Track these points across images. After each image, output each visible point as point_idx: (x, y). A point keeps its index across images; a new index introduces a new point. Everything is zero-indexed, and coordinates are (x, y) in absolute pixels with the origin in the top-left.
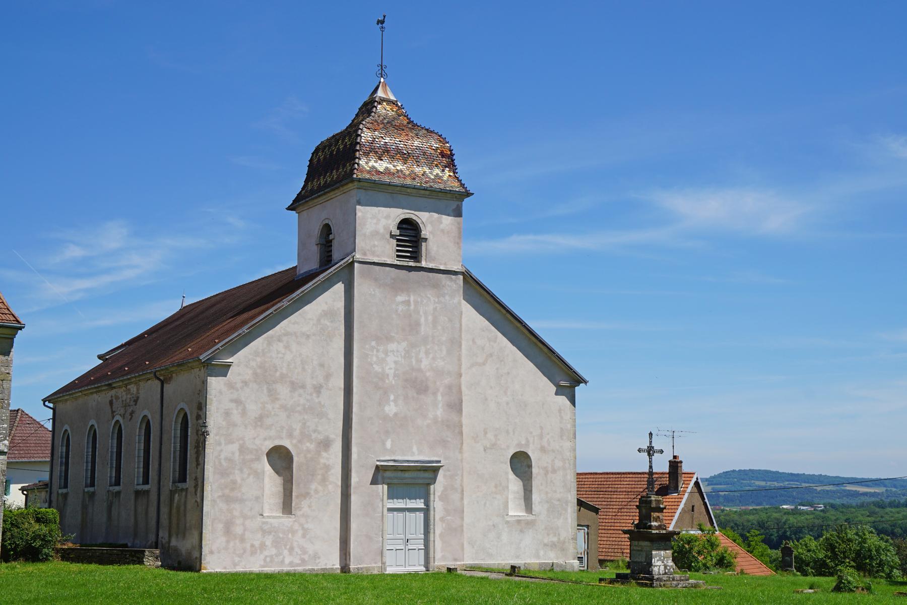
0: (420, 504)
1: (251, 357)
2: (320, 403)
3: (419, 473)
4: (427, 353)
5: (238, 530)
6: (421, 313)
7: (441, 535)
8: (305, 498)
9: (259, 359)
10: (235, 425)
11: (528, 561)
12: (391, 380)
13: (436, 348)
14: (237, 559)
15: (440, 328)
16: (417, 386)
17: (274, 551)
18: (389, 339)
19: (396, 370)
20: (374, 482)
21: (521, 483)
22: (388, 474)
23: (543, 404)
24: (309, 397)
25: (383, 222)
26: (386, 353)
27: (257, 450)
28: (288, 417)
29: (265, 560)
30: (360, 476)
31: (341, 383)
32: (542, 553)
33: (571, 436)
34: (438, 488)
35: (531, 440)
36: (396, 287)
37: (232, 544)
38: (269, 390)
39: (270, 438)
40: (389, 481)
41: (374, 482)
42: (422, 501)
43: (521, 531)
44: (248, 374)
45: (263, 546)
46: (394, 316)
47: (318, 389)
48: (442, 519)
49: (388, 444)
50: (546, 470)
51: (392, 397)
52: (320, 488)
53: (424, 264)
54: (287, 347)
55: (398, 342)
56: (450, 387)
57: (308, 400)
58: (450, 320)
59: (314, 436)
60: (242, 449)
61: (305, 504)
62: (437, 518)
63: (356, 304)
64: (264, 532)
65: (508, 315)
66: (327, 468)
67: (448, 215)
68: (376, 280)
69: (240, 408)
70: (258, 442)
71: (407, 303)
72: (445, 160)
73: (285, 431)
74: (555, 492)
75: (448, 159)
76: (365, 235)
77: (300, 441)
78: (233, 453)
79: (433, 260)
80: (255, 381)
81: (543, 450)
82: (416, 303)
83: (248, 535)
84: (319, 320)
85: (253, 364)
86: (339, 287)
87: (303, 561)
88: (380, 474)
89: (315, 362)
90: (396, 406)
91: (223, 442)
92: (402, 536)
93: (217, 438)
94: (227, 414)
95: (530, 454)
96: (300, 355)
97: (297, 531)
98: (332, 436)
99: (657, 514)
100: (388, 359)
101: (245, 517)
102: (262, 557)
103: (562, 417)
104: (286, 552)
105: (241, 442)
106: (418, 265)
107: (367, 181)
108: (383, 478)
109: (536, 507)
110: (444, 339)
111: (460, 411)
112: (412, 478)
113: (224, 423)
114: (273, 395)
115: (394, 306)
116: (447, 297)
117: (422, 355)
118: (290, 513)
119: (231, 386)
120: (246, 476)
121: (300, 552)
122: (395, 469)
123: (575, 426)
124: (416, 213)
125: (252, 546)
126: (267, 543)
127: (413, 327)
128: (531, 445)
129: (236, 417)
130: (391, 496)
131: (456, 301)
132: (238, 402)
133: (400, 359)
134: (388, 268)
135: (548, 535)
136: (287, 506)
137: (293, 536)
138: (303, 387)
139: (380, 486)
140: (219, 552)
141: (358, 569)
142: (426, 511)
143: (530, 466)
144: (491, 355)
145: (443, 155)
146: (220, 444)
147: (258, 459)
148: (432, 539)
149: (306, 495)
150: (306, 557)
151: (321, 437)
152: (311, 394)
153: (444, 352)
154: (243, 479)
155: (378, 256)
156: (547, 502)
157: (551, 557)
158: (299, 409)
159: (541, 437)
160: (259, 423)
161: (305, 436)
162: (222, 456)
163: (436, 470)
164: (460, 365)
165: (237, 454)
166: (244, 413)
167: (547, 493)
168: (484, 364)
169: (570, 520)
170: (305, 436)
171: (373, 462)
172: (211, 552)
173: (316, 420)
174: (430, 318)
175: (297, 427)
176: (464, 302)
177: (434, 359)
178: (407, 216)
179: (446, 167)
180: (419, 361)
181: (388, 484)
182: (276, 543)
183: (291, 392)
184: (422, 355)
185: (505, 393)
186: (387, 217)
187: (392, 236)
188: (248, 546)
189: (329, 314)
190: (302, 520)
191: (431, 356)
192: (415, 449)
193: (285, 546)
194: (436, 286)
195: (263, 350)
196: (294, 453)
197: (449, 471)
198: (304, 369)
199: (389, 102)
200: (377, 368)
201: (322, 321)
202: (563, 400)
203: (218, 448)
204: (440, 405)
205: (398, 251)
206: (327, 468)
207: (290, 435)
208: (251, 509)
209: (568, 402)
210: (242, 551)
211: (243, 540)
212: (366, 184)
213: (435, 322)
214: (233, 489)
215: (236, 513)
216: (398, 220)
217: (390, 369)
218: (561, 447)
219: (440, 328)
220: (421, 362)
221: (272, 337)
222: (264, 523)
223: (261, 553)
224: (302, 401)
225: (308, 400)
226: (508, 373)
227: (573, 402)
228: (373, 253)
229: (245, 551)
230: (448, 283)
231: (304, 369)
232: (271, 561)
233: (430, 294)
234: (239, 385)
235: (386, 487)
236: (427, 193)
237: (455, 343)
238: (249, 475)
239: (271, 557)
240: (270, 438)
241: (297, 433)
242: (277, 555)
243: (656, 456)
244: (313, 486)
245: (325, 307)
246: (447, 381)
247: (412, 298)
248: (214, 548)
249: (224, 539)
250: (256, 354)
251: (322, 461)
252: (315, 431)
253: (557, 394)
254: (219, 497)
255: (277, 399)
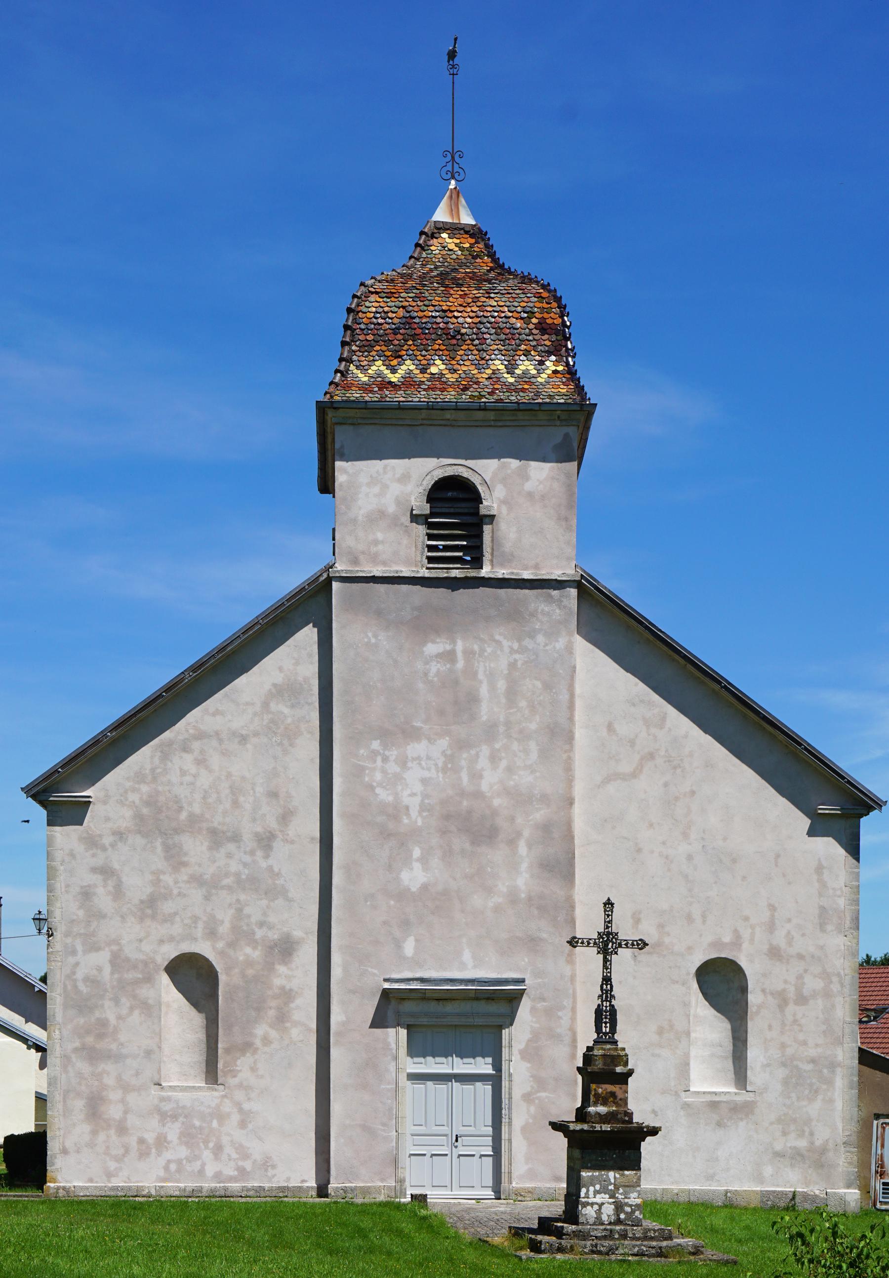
0: (483, 1066)
1: (128, 784)
2: (270, 869)
3: (475, 1004)
4: (494, 758)
5: (114, 1112)
6: (481, 676)
7: (524, 1129)
8: (244, 1055)
9: (145, 788)
10: (102, 916)
11: (735, 1187)
12: (415, 818)
13: (515, 746)
14: (112, 1165)
15: (523, 704)
16: (471, 827)
17: (183, 1152)
18: (411, 734)
19: (425, 796)
20: (379, 1021)
21: (728, 1026)
22: (409, 1007)
23: (778, 856)
24: (247, 859)
25: (396, 489)
26: (403, 763)
27: (146, 964)
28: (207, 898)
29: (166, 1168)
30: (351, 1011)
31: (314, 828)
32: (768, 1171)
33: (848, 924)
34: (518, 1035)
35: (746, 934)
36: (422, 626)
37: (102, 1137)
38: (167, 848)
39: (171, 939)
40: (411, 1021)
41: (379, 1021)
42: (489, 1060)
43: (719, 1124)
44: (124, 817)
45: (161, 1142)
46: (421, 685)
47: (266, 841)
48: (527, 1098)
49: (409, 947)
50: (782, 1000)
51: (417, 852)
52: (273, 1034)
53: (486, 571)
54: (201, 762)
55: (429, 740)
56: (546, 828)
57: (245, 865)
58: (547, 686)
59: (259, 933)
60: (118, 961)
61: (243, 1063)
62: (517, 1094)
63: (335, 666)
64: (164, 1117)
65: (690, 667)
66: (288, 995)
67: (544, 460)
68: (379, 613)
69: (111, 883)
70: (147, 947)
71: (449, 656)
72: (546, 341)
73: (200, 925)
74: (805, 1043)
75: (556, 338)
76: (354, 521)
77: (232, 945)
78: (100, 969)
79: (506, 559)
80: (139, 832)
81: (775, 953)
82: (469, 654)
83: (132, 1121)
84: (266, 705)
85: (134, 797)
86: (308, 635)
87: (243, 1173)
88: (393, 1006)
89: (259, 789)
90: (426, 867)
91: (79, 948)
92: (446, 1130)
93: (69, 940)
94: (86, 894)
95: (743, 963)
96: (229, 775)
97: (228, 1115)
98: (297, 934)
99: (610, 1088)
100: (408, 775)
101: (127, 1088)
102: (162, 1162)
103: (823, 884)
104: (207, 1155)
105: (115, 948)
106: (472, 573)
107: (363, 406)
108: (398, 1014)
109: (756, 1074)
110: (533, 726)
111: (569, 876)
112: (459, 1015)
113: (81, 913)
114: (175, 857)
115: (419, 666)
116: (540, 638)
117: (483, 763)
118: (215, 1082)
119: (92, 842)
120: (124, 1011)
121: (235, 1156)
122: (422, 996)
123: (856, 902)
124: (470, 463)
125: (141, 1141)
126: (169, 1138)
127: (460, 704)
128: (745, 945)
129: (103, 900)
130: (414, 1051)
131: (561, 644)
132: (106, 871)
133: (433, 774)
134: (404, 588)
135: (785, 1133)
136: (212, 1071)
137: (221, 1124)
138: (236, 838)
139: (391, 1031)
140: (78, 1152)
141: (345, 1190)
142: (495, 1080)
143: (744, 990)
144: (651, 756)
145: (543, 328)
146: (74, 952)
147: (149, 979)
148: (505, 1136)
149: (247, 1047)
150: (248, 1165)
151: (274, 935)
152: (252, 853)
153: (534, 755)
154: (119, 1018)
155: (384, 563)
156: (784, 1064)
157: (789, 1181)
158: (227, 881)
159: (771, 927)
160: (149, 911)
161: (241, 934)
162: (80, 975)
163: (513, 999)
164: (570, 781)
165: (107, 969)
166: (118, 893)
167: (783, 1046)
168: (634, 775)
169: (839, 1105)
170: (241, 934)
171: (377, 980)
172: (65, 1151)
173: (264, 902)
174: (502, 685)
175: (226, 917)
176: (581, 645)
177: (510, 770)
178: (450, 472)
179: (549, 353)
180: (476, 776)
181: (409, 1027)
182: (188, 1137)
183: (210, 848)
184: (483, 763)
185: (685, 835)
186: (404, 478)
187: (415, 518)
188: (133, 1141)
189: (287, 691)
190: (239, 1095)
191: (503, 764)
192: (467, 956)
193: (206, 1142)
194: (515, 616)
195: (153, 770)
196: (219, 967)
197: (543, 999)
198: (236, 804)
199: (455, 229)
200: (384, 795)
201: (273, 706)
202: (828, 848)
203: (71, 960)
204: (524, 866)
205: (431, 548)
206: (288, 995)
207: (212, 934)
208: (137, 1074)
209: (841, 852)
210: (121, 1151)
211: (122, 1129)
212: (351, 413)
213: (512, 693)
214: (100, 1036)
215: (109, 1081)
216: (429, 483)
217: (413, 795)
218: (822, 948)
219: (523, 704)
220: (481, 777)
221: (170, 743)
222: (162, 1099)
223: (159, 1154)
224: (234, 867)
225: (245, 865)
226: (693, 793)
227: (853, 849)
228: (374, 559)
229: (127, 1151)
230: (544, 607)
231: (236, 804)
232: (179, 1171)
233: (501, 633)
234: (107, 840)
235: (403, 1032)
236: (491, 415)
237: (560, 734)
238: (132, 1009)
239: (179, 1162)
240: (171, 939)
241: (224, 929)
242: (189, 1160)
243: (623, 958)
244: (261, 1030)
245: (279, 678)
246: (540, 815)
247: (460, 646)
248: (69, 1144)
249: (86, 1128)
250: (140, 777)
251: (277, 982)
252: (261, 924)
253: (812, 833)
254: (76, 1050)
255: (185, 864)
